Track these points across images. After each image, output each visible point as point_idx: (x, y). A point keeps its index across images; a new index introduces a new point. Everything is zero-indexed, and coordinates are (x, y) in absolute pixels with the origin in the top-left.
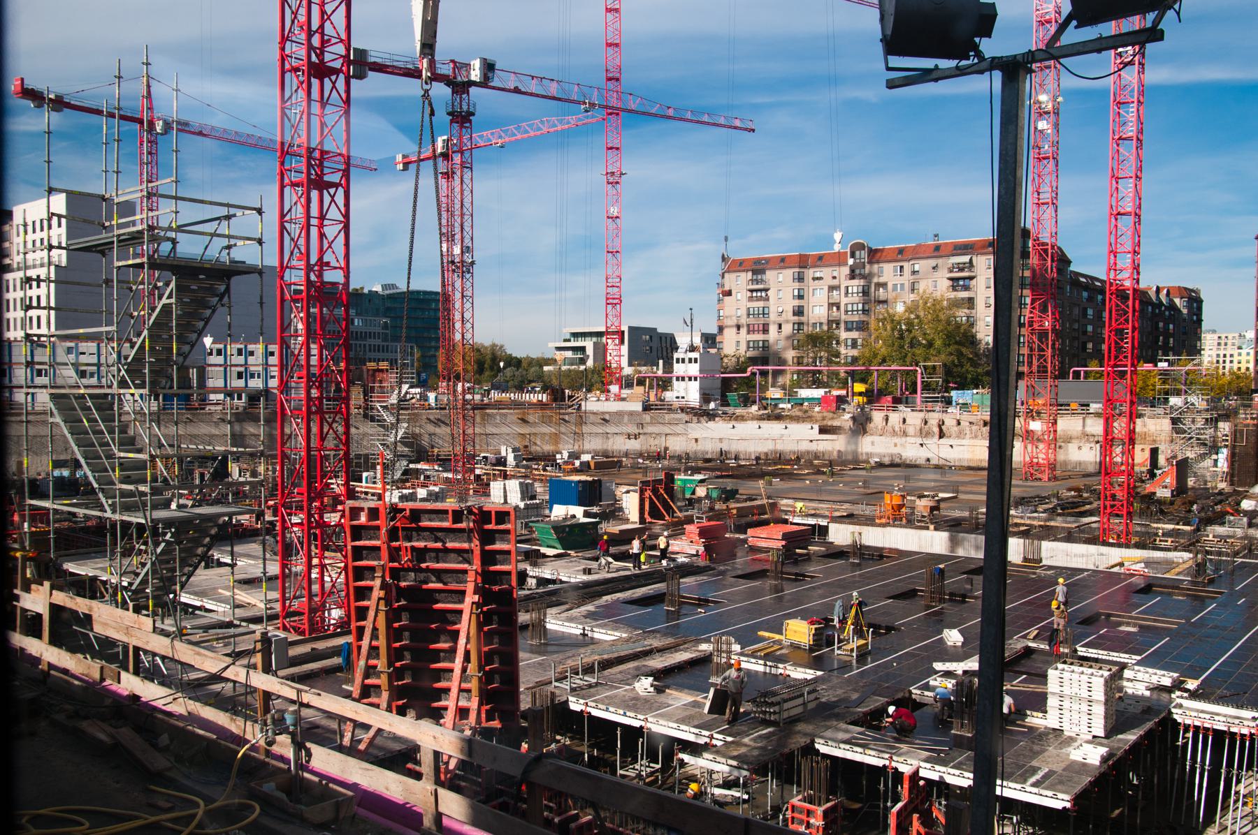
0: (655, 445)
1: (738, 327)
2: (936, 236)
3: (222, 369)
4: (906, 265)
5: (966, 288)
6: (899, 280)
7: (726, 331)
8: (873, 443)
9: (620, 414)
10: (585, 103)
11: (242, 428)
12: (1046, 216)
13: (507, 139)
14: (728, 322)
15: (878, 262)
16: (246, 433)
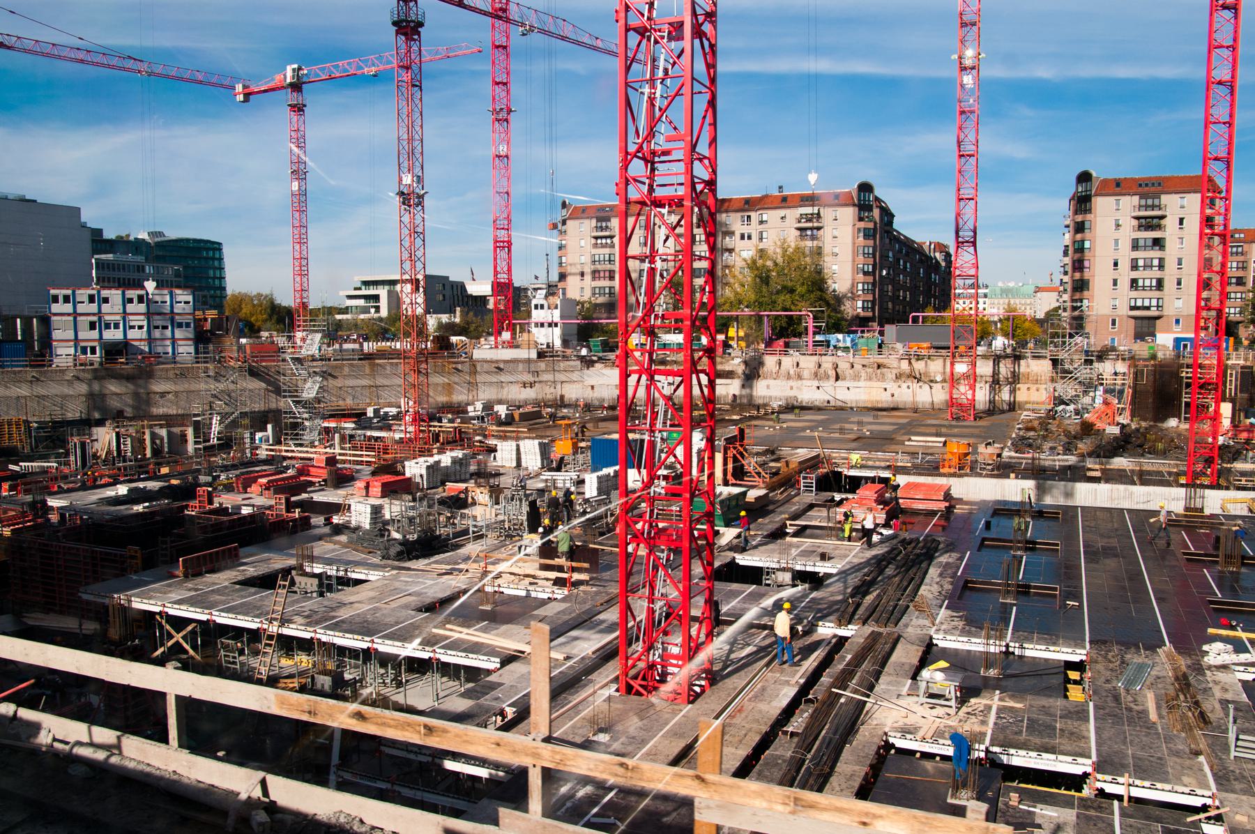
0: (549, 393)
1: (582, 274)
2: (780, 187)
3: (71, 318)
4: (753, 214)
5: (813, 238)
6: (746, 230)
7: (569, 279)
8: (768, 387)
9: (514, 361)
10: (523, 25)
11: (102, 386)
12: (967, 167)
13: (381, 67)
14: (570, 270)
15: (727, 211)
16: (107, 392)
